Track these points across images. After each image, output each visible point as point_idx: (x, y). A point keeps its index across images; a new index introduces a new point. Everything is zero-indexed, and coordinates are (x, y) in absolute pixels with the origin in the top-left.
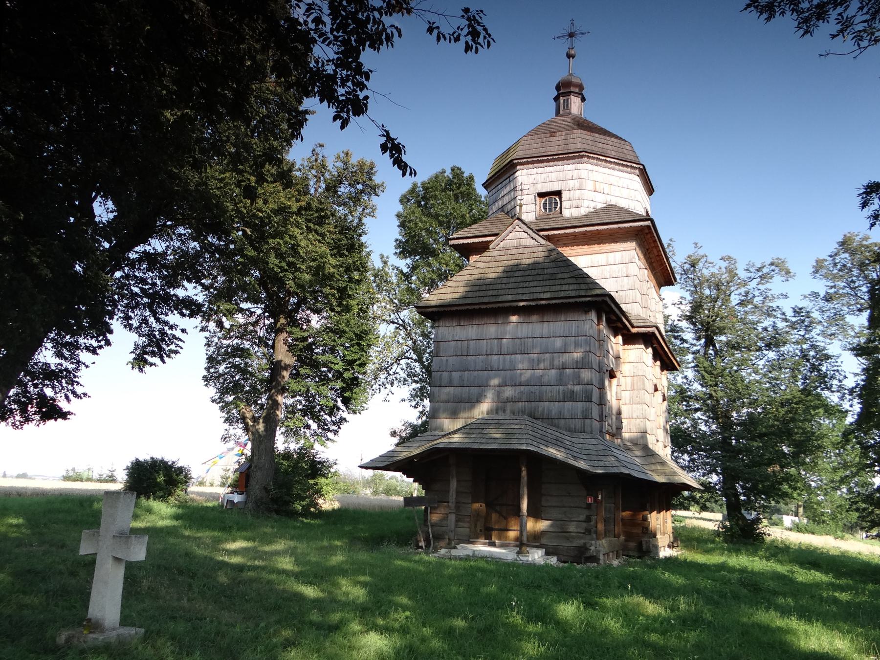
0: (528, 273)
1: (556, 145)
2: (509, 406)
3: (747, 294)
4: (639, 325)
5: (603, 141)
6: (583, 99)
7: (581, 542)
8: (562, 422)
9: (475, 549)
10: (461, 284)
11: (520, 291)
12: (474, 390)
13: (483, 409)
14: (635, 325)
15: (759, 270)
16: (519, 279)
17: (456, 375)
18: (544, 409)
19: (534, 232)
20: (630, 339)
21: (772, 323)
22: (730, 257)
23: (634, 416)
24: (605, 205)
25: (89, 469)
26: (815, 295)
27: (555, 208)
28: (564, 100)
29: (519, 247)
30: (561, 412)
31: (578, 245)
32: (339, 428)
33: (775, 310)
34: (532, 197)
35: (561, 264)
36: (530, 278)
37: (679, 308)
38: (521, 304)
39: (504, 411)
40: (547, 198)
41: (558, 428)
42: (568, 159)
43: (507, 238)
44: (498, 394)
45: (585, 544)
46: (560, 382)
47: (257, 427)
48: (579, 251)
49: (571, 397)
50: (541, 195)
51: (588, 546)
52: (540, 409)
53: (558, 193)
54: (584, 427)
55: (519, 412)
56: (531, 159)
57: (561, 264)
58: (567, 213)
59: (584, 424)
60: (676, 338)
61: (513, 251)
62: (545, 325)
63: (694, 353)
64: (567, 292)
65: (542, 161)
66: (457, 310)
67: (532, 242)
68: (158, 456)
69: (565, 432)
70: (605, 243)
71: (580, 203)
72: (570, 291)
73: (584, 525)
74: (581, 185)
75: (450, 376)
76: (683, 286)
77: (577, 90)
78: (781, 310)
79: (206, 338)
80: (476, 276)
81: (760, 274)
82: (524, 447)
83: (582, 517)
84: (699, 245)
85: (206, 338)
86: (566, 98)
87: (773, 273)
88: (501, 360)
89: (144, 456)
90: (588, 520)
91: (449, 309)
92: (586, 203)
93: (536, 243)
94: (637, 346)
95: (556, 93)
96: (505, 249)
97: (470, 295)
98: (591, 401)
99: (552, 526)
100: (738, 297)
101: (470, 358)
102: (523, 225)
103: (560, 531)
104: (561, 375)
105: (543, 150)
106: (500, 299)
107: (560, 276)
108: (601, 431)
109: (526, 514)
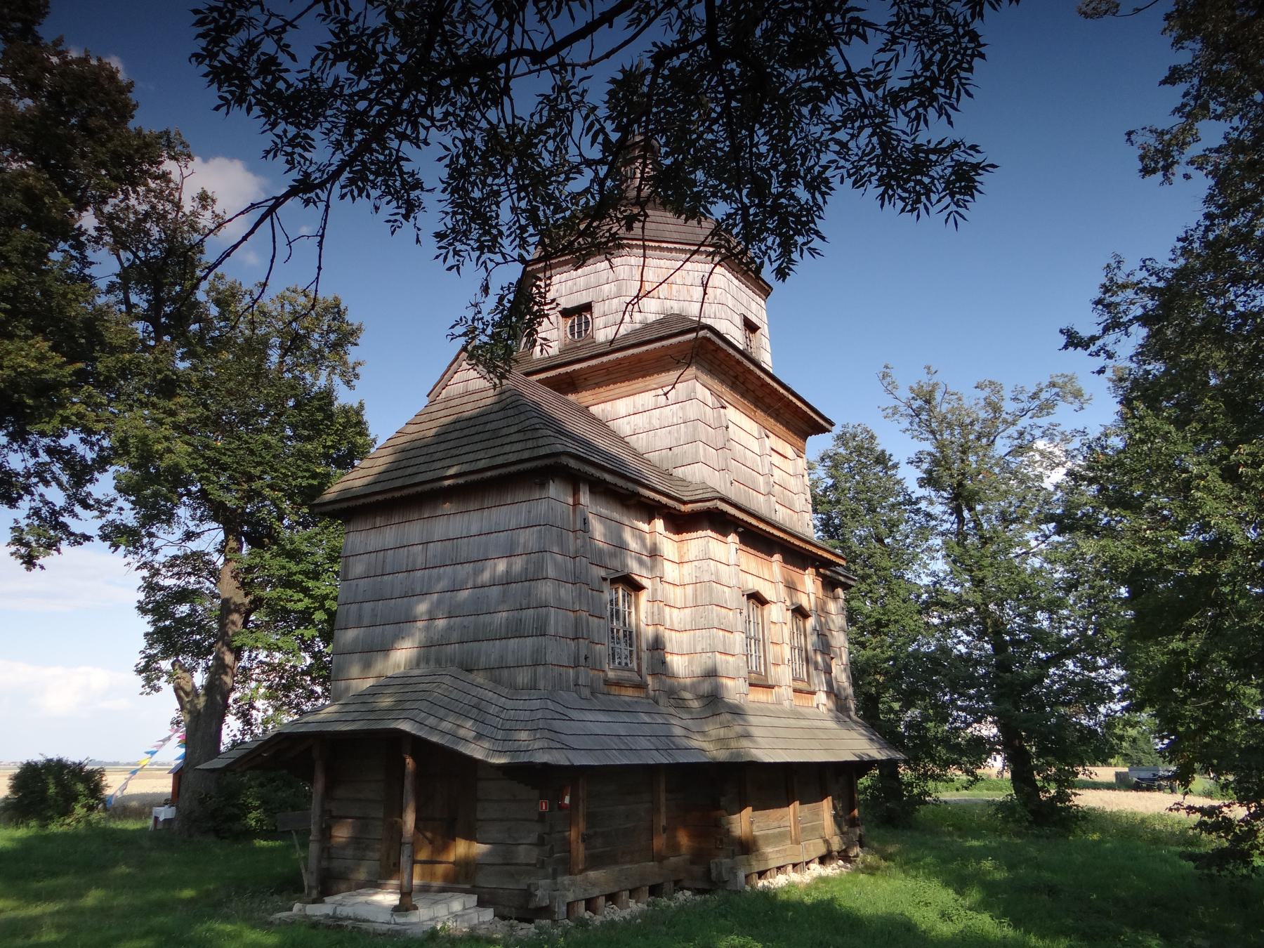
3: (1021, 434)
5: (659, 219)
8: (505, 672)
13: (402, 655)
14: (685, 499)
15: (1035, 396)
16: (452, 444)
20: (681, 523)
22: (991, 383)
23: (699, 650)
24: (662, 316)
27: (586, 330)
31: (615, 383)
35: (511, 412)
36: (465, 441)
37: (918, 467)
38: (447, 483)
43: (451, 382)
45: (529, 886)
48: (617, 391)
51: (532, 889)
53: (587, 307)
54: (535, 682)
55: (446, 662)
59: (535, 674)
62: (486, 512)
63: (943, 534)
68: (53, 755)
69: (505, 691)
70: (652, 374)
72: (513, 452)
74: (619, 289)
75: (360, 609)
79: (144, 578)
81: (1037, 402)
83: (533, 838)
84: (933, 370)
85: (144, 578)
89: (37, 755)
94: (700, 533)
96: (448, 399)
100: (1008, 442)
101: (385, 578)
103: (505, 862)
104: (505, 592)
107: (505, 431)
108: (576, 685)
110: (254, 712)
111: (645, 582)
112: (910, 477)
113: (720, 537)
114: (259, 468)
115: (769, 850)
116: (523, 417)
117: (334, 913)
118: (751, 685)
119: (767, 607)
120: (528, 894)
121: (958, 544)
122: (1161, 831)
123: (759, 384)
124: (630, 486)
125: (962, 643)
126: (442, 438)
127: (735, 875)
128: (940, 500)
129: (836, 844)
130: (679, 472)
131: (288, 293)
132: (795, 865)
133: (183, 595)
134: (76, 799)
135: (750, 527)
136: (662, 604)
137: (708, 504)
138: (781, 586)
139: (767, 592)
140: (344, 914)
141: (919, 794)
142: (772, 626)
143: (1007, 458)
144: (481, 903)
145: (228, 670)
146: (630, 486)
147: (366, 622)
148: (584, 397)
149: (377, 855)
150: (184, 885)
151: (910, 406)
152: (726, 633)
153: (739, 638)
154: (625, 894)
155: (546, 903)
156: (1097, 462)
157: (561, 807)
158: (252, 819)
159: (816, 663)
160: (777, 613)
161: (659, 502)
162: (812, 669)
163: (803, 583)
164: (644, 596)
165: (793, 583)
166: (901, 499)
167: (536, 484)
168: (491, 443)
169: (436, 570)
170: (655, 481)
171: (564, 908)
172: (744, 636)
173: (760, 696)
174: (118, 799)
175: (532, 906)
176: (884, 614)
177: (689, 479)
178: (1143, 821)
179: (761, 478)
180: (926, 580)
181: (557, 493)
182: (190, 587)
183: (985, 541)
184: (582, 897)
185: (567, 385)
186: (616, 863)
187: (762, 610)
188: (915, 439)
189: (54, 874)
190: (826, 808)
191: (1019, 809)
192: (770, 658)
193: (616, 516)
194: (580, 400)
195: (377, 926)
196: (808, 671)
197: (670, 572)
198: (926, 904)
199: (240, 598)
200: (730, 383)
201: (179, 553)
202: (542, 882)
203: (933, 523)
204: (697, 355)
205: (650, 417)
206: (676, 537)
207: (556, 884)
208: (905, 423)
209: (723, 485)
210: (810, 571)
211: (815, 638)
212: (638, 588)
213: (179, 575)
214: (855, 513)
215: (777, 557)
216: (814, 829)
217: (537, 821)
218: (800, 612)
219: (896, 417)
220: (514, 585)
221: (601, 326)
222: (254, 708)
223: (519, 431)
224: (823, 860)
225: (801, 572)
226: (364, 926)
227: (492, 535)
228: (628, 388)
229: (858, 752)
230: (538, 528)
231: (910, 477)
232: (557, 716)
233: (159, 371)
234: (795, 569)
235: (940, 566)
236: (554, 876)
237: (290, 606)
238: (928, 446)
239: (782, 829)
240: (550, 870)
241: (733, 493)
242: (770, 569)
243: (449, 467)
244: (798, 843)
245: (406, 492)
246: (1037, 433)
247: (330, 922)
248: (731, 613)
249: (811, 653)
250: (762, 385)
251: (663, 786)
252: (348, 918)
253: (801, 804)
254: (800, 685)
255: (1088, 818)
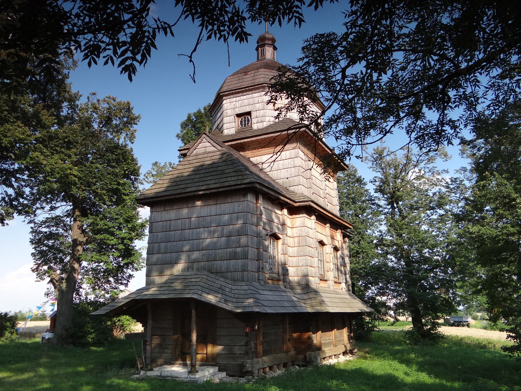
0: (208, 170)
1: (247, 80)
2: (195, 265)
4: (300, 200)
6: (275, 48)
7: (239, 362)
9: (261, 351)
10: (167, 181)
11: (201, 184)
12: (174, 255)
13: (179, 268)
14: (296, 201)
17: (163, 245)
18: (217, 266)
19: (214, 142)
20: (294, 211)
21: (438, 190)
23: (300, 265)
25: (30, 311)
26: (464, 170)
27: (248, 124)
28: (261, 50)
29: (206, 153)
30: (228, 267)
31: (262, 148)
32: (128, 281)
33: (441, 181)
34: (233, 117)
35: (229, 163)
36: (208, 174)
37: (374, 184)
38: (201, 193)
39: (193, 269)
40: (243, 117)
41: (227, 278)
42: (255, 89)
43: (198, 147)
44: (189, 256)
45: (243, 362)
46: (227, 246)
47: (61, 285)
48: (263, 152)
49: (234, 257)
50: (239, 115)
51: (245, 363)
52: (215, 266)
53: (249, 113)
55: (202, 269)
56: (231, 92)
57: (229, 163)
58: (255, 127)
60: (373, 204)
61: (201, 156)
62: (219, 206)
63: (385, 214)
64: (229, 182)
65: (239, 93)
66: (161, 200)
67: (213, 149)
69: (230, 282)
71: (263, 119)
72: (231, 181)
73: (244, 348)
75: (159, 246)
76: (375, 169)
77: (270, 42)
78: (445, 181)
79: (32, 228)
80: (175, 176)
82: (189, 296)
83: (243, 343)
85: (32, 228)
86: (262, 48)
87: (437, 156)
88: (191, 233)
90: (247, 344)
91: (156, 199)
92: (267, 119)
93: (216, 149)
94: (301, 215)
95: (257, 45)
96: (197, 155)
97: (170, 188)
98: (247, 259)
99: (223, 350)
101: (171, 232)
102: (207, 138)
103: (230, 353)
105: (239, 85)
106: (189, 190)
107: (227, 171)
108: (259, 279)
109: (195, 344)
110: (81, 290)
111: (280, 236)
112: (371, 188)
113: (309, 217)
114: (95, 180)
115: (325, 349)
116: (235, 165)
117: (161, 374)
118: (321, 280)
119: (325, 246)
120: (242, 366)
121: (392, 219)
122: (470, 344)
123: (322, 150)
124: (277, 195)
125: (392, 261)
126: (196, 172)
127: (317, 359)
128: (383, 198)
129: (349, 347)
130: (292, 189)
131: (107, 99)
132: (335, 355)
133: (50, 236)
134: (6, 330)
135: (321, 213)
136: (287, 245)
137: (306, 203)
138: (330, 237)
139: (325, 241)
140: (166, 375)
141: (372, 327)
142: (326, 255)
143: (413, 181)
144: (220, 370)
145: (76, 271)
146: (277, 195)
147: (162, 250)
148: (248, 154)
149: (170, 351)
150: (80, 365)
151: (373, 157)
152: (311, 258)
153: (316, 260)
154: (275, 366)
155: (250, 369)
156: (476, 194)
157: (254, 330)
158: (90, 338)
159: (341, 271)
160: (328, 249)
161: (287, 202)
162: (340, 273)
163: (336, 236)
164: (280, 242)
165: (333, 236)
166: (367, 198)
167: (242, 194)
168: (221, 176)
169: (195, 230)
170: (284, 193)
171: (257, 371)
172: (317, 259)
173: (323, 284)
174: (23, 328)
175: (244, 370)
176: (360, 249)
177: (296, 192)
178: (461, 339)
179: (321, 191)
180: (377, 234)
181: (250, 198)
182: (53, 232)
183: (404, 218)
184: (261, 367)
185: (241, 148)
186: (272, 354)
187: (323, 248)
188: (374, 171)
189: (17, 362)
190: (345, 332)
191: (416, 333)
192: (326, 269)
193: (270, 208)
194: (246, 155)
195: (183, 379)
196: (338, 274)
197: (289, 231)
198: (397, 370)
199: (82, 239)
200: (311, 150)
201: (50, 216)
202: (248, 361)
203: (381, 209)
204: (300, 138)
205: (278, 164)
206: (290, 217)
207: (253, 362)
208: (370, 164)
209: (309, 195)
210: (339, 231)
211: (341, 260)
212: (278, 238)
213: (48, 227)
214: (347, 204)
215: (328, 225)
216: (340, 340)
217: (244, 336)
218: (336, 249)
219: (366, 161)
220: (233, 237)
221: (255, 122)
222: (81, 288)
223: (234, 172)
224: (345, 353)
225: (335, 231)
226: (177, 379)
227: (222, 216)
228: (268, 151)
229: (360, 308)
230: (243, 213)
231: (371, 188)
232: (256, 293)
233: (66, 138)
234: (333, 230)
235: (384, 228)
236: (252, 358)
237: (108, 242)
238: (379, 175)
239: (330, 341)
240: (251, 356)
241: (314, 198)
242: (325, 230)
243: (202, 186)
244: (336, 346)
245: (182, 196)
246: (427, 170)
247: (160, 378)
248: (313, 249)
249: (339, 266)
250: (324, 150)
251: (288, 322)
252: (168, 376)
253: (322, 332)
254: (336, 280)
255: (442, 337)
